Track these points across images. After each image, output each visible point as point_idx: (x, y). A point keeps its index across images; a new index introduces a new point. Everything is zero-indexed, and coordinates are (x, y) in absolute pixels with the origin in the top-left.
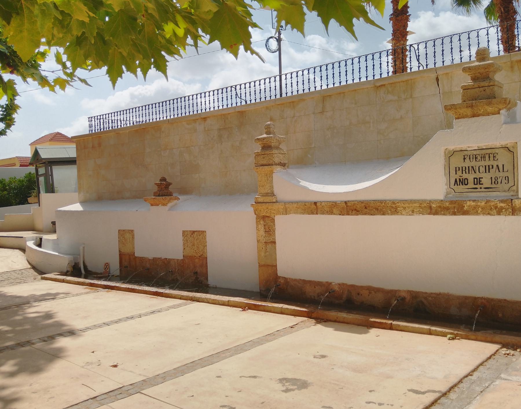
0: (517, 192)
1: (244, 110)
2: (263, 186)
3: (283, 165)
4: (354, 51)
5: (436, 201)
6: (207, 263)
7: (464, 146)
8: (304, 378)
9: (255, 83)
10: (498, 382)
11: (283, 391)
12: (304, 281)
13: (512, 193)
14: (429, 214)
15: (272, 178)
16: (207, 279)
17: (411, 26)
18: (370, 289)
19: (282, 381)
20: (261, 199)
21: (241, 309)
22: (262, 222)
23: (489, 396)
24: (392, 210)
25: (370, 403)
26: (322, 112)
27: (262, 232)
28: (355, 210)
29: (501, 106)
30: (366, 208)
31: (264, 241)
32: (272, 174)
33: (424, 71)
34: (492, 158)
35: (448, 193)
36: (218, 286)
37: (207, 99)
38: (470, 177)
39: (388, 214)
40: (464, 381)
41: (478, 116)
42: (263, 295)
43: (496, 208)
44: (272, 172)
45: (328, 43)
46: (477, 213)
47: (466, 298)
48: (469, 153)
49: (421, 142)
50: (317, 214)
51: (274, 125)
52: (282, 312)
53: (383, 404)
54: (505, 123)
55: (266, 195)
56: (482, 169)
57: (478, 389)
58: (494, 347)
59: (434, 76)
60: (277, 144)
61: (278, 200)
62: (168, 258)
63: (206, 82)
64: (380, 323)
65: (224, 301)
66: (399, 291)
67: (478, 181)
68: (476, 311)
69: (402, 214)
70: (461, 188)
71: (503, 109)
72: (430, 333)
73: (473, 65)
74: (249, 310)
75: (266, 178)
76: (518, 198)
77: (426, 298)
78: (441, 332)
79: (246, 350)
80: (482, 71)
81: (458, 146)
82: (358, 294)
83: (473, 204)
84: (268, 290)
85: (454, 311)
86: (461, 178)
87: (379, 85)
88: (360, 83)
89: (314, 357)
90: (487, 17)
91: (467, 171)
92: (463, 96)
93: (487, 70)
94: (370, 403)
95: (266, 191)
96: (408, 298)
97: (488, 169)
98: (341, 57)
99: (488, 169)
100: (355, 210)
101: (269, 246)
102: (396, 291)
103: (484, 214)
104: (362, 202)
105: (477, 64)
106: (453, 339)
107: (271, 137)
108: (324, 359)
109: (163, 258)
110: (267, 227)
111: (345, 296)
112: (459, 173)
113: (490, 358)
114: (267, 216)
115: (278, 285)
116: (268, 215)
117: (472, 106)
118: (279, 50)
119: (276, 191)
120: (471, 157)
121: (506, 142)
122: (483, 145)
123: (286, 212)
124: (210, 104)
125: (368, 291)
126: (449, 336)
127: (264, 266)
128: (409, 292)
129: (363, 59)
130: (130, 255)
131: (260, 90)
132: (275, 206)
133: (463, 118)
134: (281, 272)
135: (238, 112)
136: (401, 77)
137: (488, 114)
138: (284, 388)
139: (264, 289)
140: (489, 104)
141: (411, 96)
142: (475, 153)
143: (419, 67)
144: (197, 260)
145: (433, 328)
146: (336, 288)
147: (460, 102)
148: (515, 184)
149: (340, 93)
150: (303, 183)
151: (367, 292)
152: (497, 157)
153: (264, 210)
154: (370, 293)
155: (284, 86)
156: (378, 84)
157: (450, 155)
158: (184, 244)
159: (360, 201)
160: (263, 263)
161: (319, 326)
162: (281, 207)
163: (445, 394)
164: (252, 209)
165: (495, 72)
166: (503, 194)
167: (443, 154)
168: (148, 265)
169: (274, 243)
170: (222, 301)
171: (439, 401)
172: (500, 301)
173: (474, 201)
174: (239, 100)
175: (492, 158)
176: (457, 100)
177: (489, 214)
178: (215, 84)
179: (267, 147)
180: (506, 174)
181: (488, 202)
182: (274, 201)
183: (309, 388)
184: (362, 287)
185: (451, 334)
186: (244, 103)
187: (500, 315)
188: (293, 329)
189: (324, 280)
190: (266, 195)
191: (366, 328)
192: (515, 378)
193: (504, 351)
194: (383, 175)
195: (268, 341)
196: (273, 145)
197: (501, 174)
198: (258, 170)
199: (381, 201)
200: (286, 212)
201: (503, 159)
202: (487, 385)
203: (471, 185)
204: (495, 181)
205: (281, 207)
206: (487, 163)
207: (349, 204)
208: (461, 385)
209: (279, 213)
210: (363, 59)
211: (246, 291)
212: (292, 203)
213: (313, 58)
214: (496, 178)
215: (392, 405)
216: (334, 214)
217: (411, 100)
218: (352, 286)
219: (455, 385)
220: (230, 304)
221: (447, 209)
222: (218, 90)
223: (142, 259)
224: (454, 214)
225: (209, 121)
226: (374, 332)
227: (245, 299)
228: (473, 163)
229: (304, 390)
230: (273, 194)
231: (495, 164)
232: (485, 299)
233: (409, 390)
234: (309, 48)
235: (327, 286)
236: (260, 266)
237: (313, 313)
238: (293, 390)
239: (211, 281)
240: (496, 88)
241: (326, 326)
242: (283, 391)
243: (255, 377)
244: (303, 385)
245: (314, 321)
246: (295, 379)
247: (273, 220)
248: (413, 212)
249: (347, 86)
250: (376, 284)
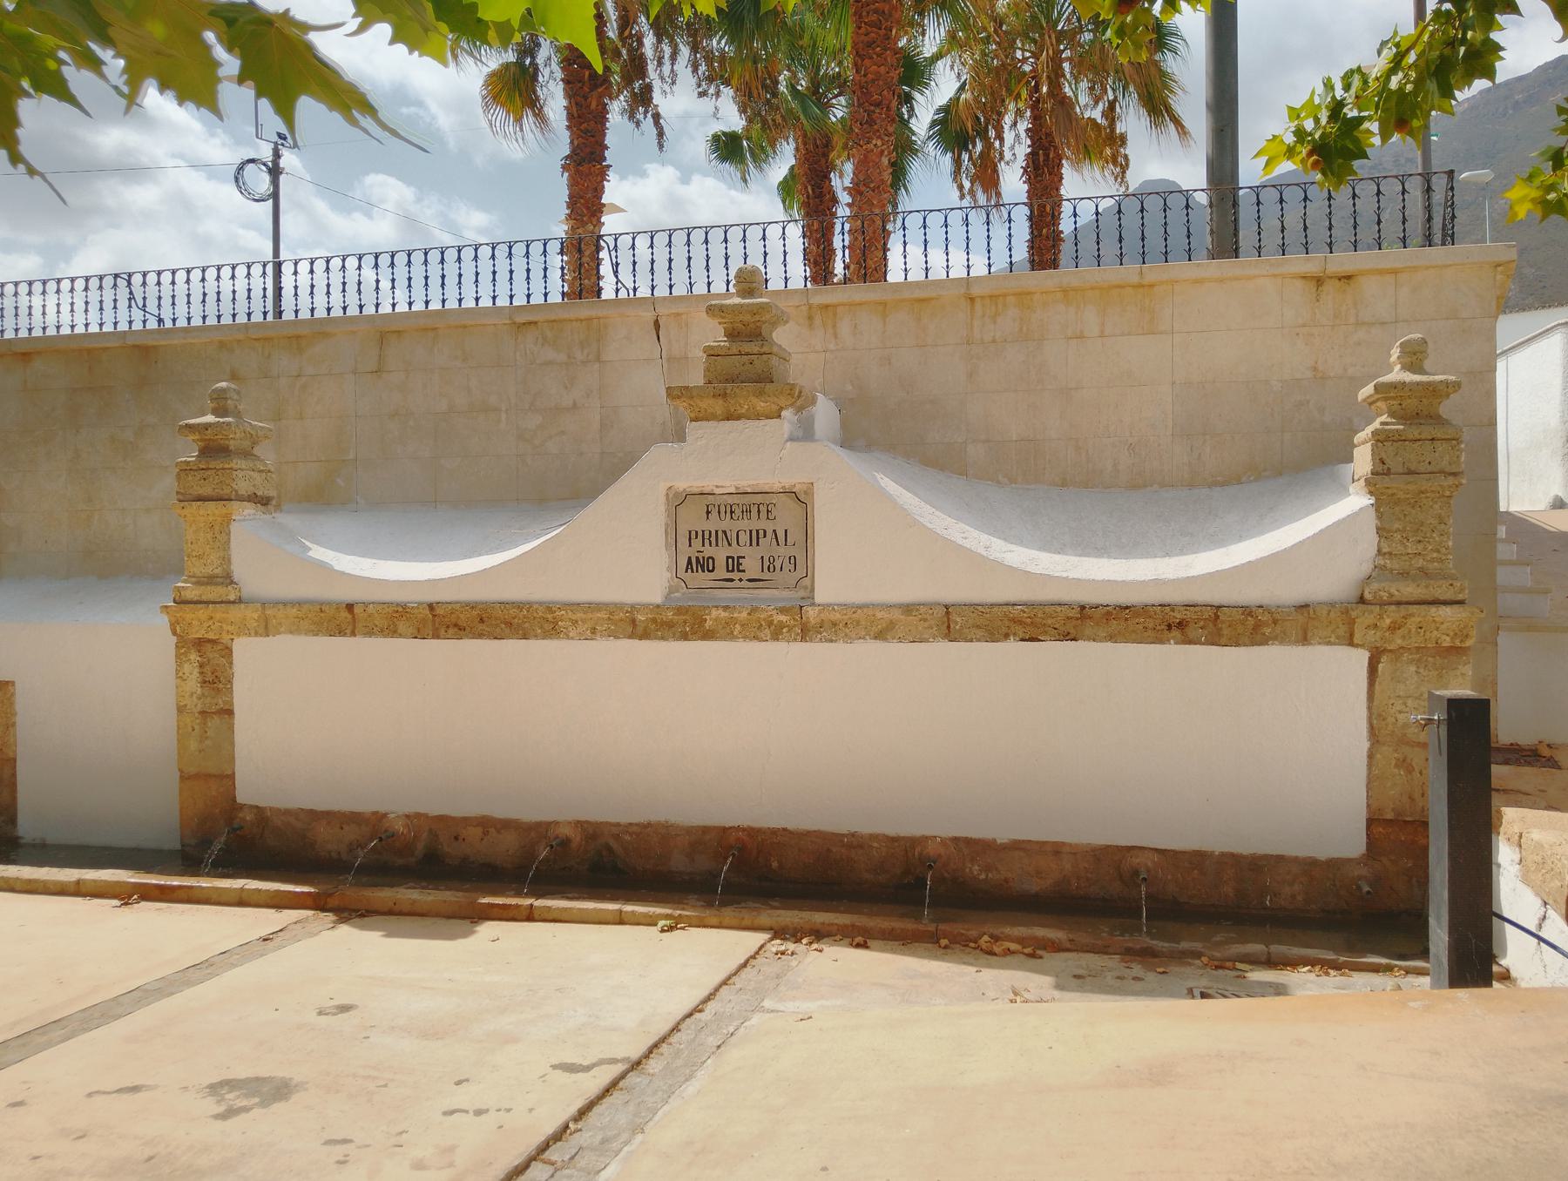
0: (813, 590)
1: (151, 343)
2: (199, 557)
3: (263, 501)
4: (481, 231)
5: (645, 606)
6: (14, 775)
7: (707, 484)
8: (281, 1073)
9: (219, 270)
10: (756, 1019)
11: (218, 1117)
13: (802, 593)
14: (630, 637)
15: (229, 534)
16: (13, 820)
17: (614, 191)
18: (485, 823)
19: (214, 1089)
20: (192, 593)
21: (116, 902)
22: (194, 656)
23: (734, 1055)
24: (548, 626)
25: (452, 1112)
26: (378, 371)
27: (193, 683)
28: (456, 625)
29: (783, 401)
30: (482, 621)
31: (199, 708)
32: (228, 524)
33: (629, 300)
34: (763, 514)
35: (672, 590)
37: (37, 301)
38: (720, 554)
39: (536, 637)
40: (682, 1027)
41: (738, 418)
42: (190, 859)
43: (770, 624)
44: (227, 520)
45: (419, 200)
46: (731, 636)
47: (705, 830)
48: (719, 500)
49: (614, 467)
50: (353, 634)
51: (238, 393)
52: (242, 900)
53: (487, 1111)
54: (791, 439)
55: (210, 580)
56: (744, 538)
57: (713, 1041)
58: (754, 939)
59: (649, 316)
60: (247, 443)
61: (245, 594)
63: (67, 254)
64: (504, 906)
65: (61, 883)
66: (557, 823)
67: (735, 564)
68: (726, 858)
69: (568, 638)
70: (702, 578)
71: (786, 407)
72: (620, 920)
73: (728, 302)
74: (143, 903)
75: (209, 536)
76: (813, 604)
77: (617, 837)
78: (646, 915)
79: (120, 1017)
80: (747, 318)
81: (696, 484)
82: (456, 838)
83: (724, 614)
84: (205, 843)
85: (678, 863)
86: (700, 556)
87: (523, 322)
88: (477, 311)
89: (320, 1013)
90: (784, 202)
91: (713, 539)
92: (707, 370)
93: (757, 318)
94: (452, 1112)
95: (209, 570)
96: (577, 838)
97: (756, 537)
98: (447, 240)
99: (756, 537)
100: (456, 625)
101: (214, 722)
102: (548, 824)
103: (745, 637)
104: (472, 606)
105: (737, 300)
106: (671, 929)
107: (229, 424)
108: (345, 1015)
110: (208, 669)
111: (420, 847)
112: (697, 543)
113: (744, 965)
114: (209, 641)
115: (235, 830)
116: (211, 636)
117: (724, 395)
118: (275, 196)
119: (238, 570)
120: (723, 509)
121: (793, 481)
122: (746, 483)
123: (266, 627)
124: (60, 315)
125: (479, 831)
126: (662, 923)
127: (197, 776)
128: (579, 824)
129: (501, 252)
131: (205, 294)
132: (235, 613)
133: (707, 420)
134: (245, 794)
135: (135, 346)
136: (584, 309)
137: (758, 417)
138: (221, 1109)
139: (193, 842)
140: (760, 394)
141: (598, 359)
142: (730, 500)
143: (617, 290)
145: (629, 908)
146: (399, 827)
147: (701, 382)
148: (809, 573)
149: (425, 330)
150: (319, 553)
151: (478, 831)
152: (774, 512)
153: (199, 623)
154: (486, 833)
155: (288, 291)
156: (520, 319)
157: (679, 501)
159: (467, 604)
160: (192, 770)
161: (344, 929)
162: (251, 614)
163: (636, 1065)
164: (163, 621)
165: (774, 325)
166: (786, 593)
167: (663, 499)
169: (230, 712)
170: (56, 883)
171: (621, 1084)
172: (774, 832)
173: (726, 608)
174: (137, 315)
175: (763, 514)
176: (696, 378)
177: (756, 638)
178: (94, 258)
179: (214, 449)
180: (792, 551)
181: (754, 610)
182: (232, 597)
183: (295, 1098)
184: (465, 819)
185: (667, 917)
186: (152, 324)
187: (775, 865)
188: (270, 944)
189: (366, 806)
190: (210, 580)
191: (467, 922)
192: (790, 1006)
193: (777, 945)
194: (527, 541)
195: (190, 984)
196: (232, 445)
197: (782, 550)
198: (185, 512)
199: (519, 605)
200: (266, 627)
201: (787, 516)
202: (731, 1029)
203: (720, 572)
204: (769, 565)
205: (251, 614)
206: (755, 524)
207: (439, 611)
208: (674, 1039)
209: (244, 630)
210: (501, 252)
211: (138, 851)
212: (285, 604)
213: (380, 232)
214: (772, 560)
215: (508, 1110)
216: (401, 636)
217: (597, 366)
218: (442, 819)
219: (663, 1039)
220: (84, 890)
221: (670, 625)
222: (87, 279)
224: (685, 637)
226: (488, 930)
227: (130, 873)
228: (727, 524)
229: (278, 1107)
230: (228, 579)
231: (769, 527)
232: (744, 830)
233: (554, 1067)
234: (369, 207)
235: (374, 823)
236: (185, 778)
237: (330, 895)
238: (246, 1109)
239: (27, 827)
240: (774, 361)
241: (362, 928)
242: (218, 1117)
243: (135, 1089)
244: (276, 1091)
245: (331, 917)
246: (257, 1079)
247: (228, 651)
248: (594, 631)
249: (443, 313)
250: (500, 812)
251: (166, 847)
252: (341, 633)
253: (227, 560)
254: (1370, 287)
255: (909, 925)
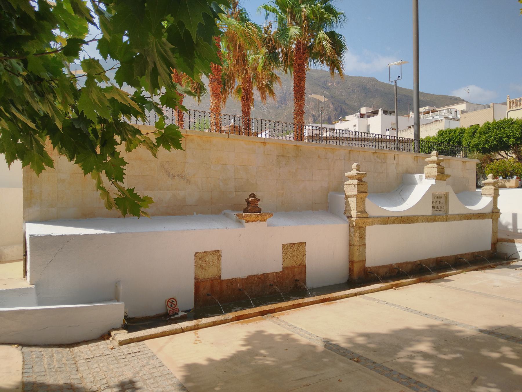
6: (306, 270)
12: (379, 266)
16: (305, 283)
36: (314, 287)
62: (266, 272)
101: (362, 247)
109: (260, 274)
119: (367, 209)
130: (212, 280)
144: (296, 269)
158: (283, 257)
168: (239, 286)
169: (365, 245)
199: (414, 216)
223: (231, 282)
224: (433, 222)
225: (268, 146)
241: (242, 323)
251: (341, 282)
252: (385, 224)
253: (364, 207)
254: (467, 163)
255: (481, 266)
